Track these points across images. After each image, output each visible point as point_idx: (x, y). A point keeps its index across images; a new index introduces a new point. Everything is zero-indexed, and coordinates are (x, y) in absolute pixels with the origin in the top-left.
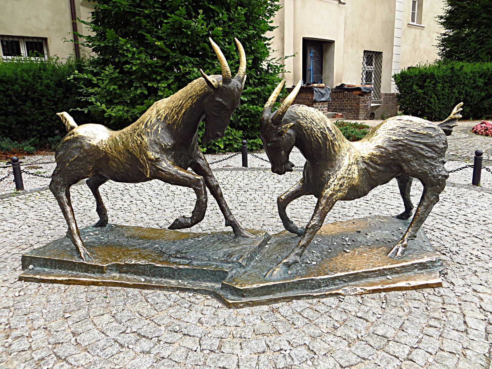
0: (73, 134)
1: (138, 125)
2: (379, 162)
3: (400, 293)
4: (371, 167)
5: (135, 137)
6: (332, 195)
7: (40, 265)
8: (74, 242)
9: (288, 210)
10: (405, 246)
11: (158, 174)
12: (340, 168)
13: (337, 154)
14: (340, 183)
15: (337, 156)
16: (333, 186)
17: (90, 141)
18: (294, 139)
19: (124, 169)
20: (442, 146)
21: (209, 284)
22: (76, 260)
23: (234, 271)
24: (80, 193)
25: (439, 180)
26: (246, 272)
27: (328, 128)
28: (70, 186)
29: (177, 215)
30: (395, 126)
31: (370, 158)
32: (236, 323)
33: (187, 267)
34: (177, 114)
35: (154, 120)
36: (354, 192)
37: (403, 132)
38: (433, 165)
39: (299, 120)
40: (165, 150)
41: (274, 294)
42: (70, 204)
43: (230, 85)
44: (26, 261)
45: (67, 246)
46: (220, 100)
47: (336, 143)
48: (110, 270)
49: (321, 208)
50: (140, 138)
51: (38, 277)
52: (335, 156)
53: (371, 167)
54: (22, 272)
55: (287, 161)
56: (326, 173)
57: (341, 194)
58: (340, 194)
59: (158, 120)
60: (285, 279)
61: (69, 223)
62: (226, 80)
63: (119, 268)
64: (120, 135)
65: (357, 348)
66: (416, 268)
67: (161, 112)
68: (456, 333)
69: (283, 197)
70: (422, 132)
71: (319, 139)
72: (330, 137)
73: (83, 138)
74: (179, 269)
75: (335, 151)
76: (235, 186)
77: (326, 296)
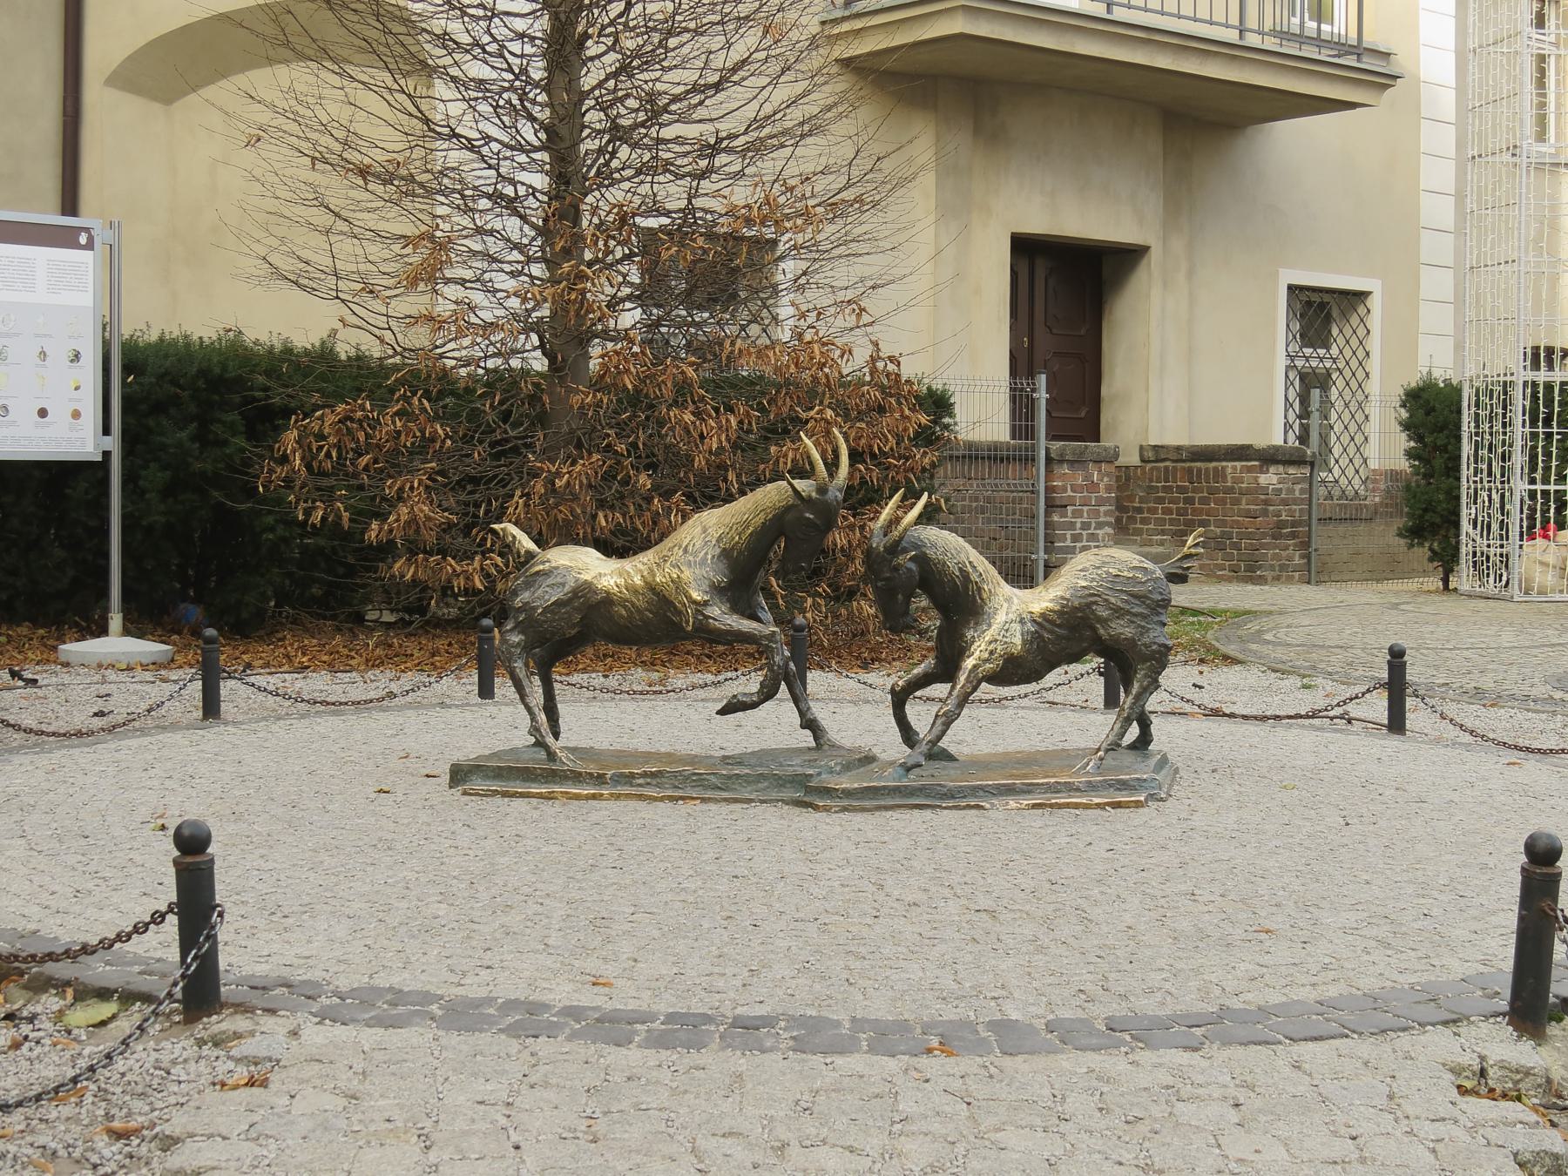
12: (990, 626)
14: (991, 647)
31: (1043, 615)
36: (1016, 670)
56: (969, 634)
62: (822, 490)
72: (974, 577)
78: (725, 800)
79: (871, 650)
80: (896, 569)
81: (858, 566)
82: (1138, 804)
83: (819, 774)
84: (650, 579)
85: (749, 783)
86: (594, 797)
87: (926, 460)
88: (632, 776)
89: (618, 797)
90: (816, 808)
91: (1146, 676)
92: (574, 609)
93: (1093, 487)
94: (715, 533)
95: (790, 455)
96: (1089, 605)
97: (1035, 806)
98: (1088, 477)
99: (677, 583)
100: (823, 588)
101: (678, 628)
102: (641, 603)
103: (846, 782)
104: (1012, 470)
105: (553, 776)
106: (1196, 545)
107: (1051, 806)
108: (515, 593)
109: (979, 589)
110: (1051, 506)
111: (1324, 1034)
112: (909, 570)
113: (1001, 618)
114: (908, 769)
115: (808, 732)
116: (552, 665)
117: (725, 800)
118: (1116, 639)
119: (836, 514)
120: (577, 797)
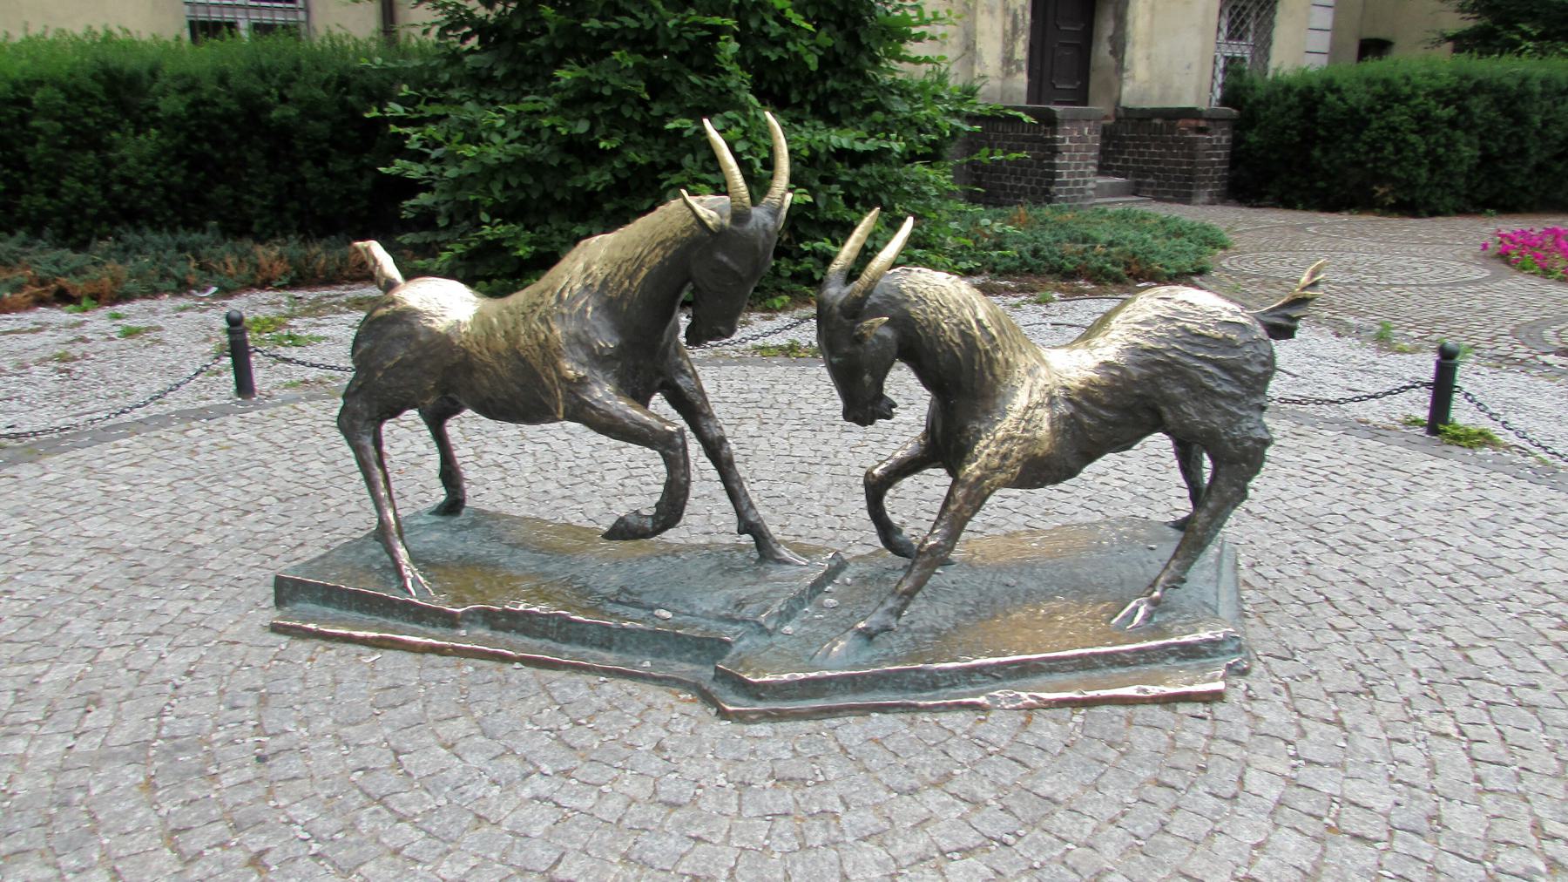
0: (394, 302)
1: (542, 293)
2: (1106, 400)
3: (1122, 710)
4: (1086, 412)
5: (536, 325)
6: (980, 479)
7: (311, 599)
8: (391, 551)
9: (889, 502)
10: (1155, 602)
11: (581, 412)
12: (1004, 414)
13: (999, 382)
14: (1003, 449)
20: (1258, 369)
21: (687, 667)
22: (399, 597)
23: (746, 642)
24: (406, 436)
25: (1246, 450)
26: (772, 645)
27: (979, 322)
28: (382, 421)
29: (621, 509)
30: (1151, 314)
31: (1082, 392)
32: (736, 755)
33: (640, 625)
38: (1233, 414)
39: (906, 306)
40: (599, 360)
41: (829, 698)
42: (381, 465)
43: (750, 226)
44: (286, 590)
45: (373, 557)
46: (725, 259)
47: (1000, 355)
48: (471, 621)
49: (953, 507)
50: (544, 328)
51: (312, 626)
53: (1086, 412)
54: (278, 613)
55: (880, 396)
58: (1000, 476)
59: (586, 288)
60: (856, 666)
61: (379, 508)
62: (739, 216)
63: (490, 618)
64: (500, 314)
65: (984, 819)
66: (1172, 654)
68: (1211, 800)
69: (876, 472)
70: (1212, 332)
72: (983, 344)
73: (415, 313)
74: (624, 629)
75: (994, 375)
76: (790, 416)
77: (948, 708)
93: (1082, 139)
98: (1081, 131)
109: (991, 361)
112: (881, 339)
113: (1020, 401)
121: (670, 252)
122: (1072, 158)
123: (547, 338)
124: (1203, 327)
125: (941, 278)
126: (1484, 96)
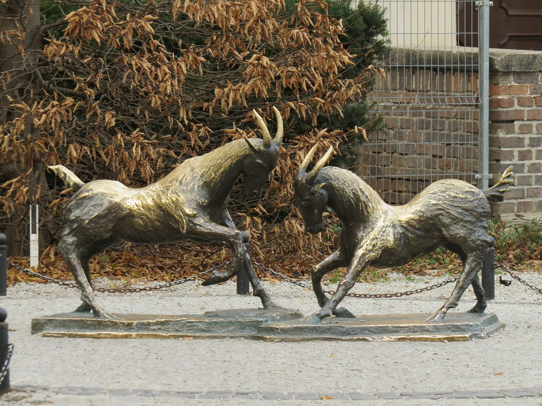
12: (373, 229)
13: (370, 215)
14: (373, 243)
15: (371, 218)
16: (365, 246)
17: (112, 197)
18: (327, 199)
19: (153, 227)
27: (360, 189)
31: (407, 222)
34: (215, 172)
35: (189, 178)
36: (389, 259)
37: (443, 196)
39: (331, 181)
47: (370, 205)
50: (175, 195)
52: (368, 217)
53: (409, 231)
56: (360, 234)
57: (374, 254)
62: (267, 145)
67: (196, 170)
70: (460, 196)
71: (352, 200)
72: (363, 198)
78: (208, 337)
79: (301, 265)
80: (313, 194)
81: (289, 190)
82: (465, 339)
83: (266, 321)
84: (158, 201)
85: (223, 327)
86: (126, 337)
87: (351, 92)
88: (149, 324)
89: (141, 336)
90: (264, 339)
91: (473, 261)
92: (109, 220)
94: (199, 172)
95: (232, 95)
96: (437, 216)
97: (400, 340)
99: (176, 203)
100: (260, 208)
101: (177, 231)
102: (152, 216)
103: (283, 325)
104: (457, 82)
105: (100, 325)
106: (509, 177)
107: (410, 339)
108: (70, 211)
109: (366, 206)
110: (496, 121)
111: (495, 396)
112: (322, 194)
113: (380, 224)
114: (322, 318)
115: (259, 299)
116: (89, 258)
117: (208, 337)
118: (454, 237)
119: (276, 160)
120: (116, 337)
121: (235, 161)
122: (524, 156)
123: (177, 200)
124: (457, 194)
125: (345, 171)
126: (488, 206)
